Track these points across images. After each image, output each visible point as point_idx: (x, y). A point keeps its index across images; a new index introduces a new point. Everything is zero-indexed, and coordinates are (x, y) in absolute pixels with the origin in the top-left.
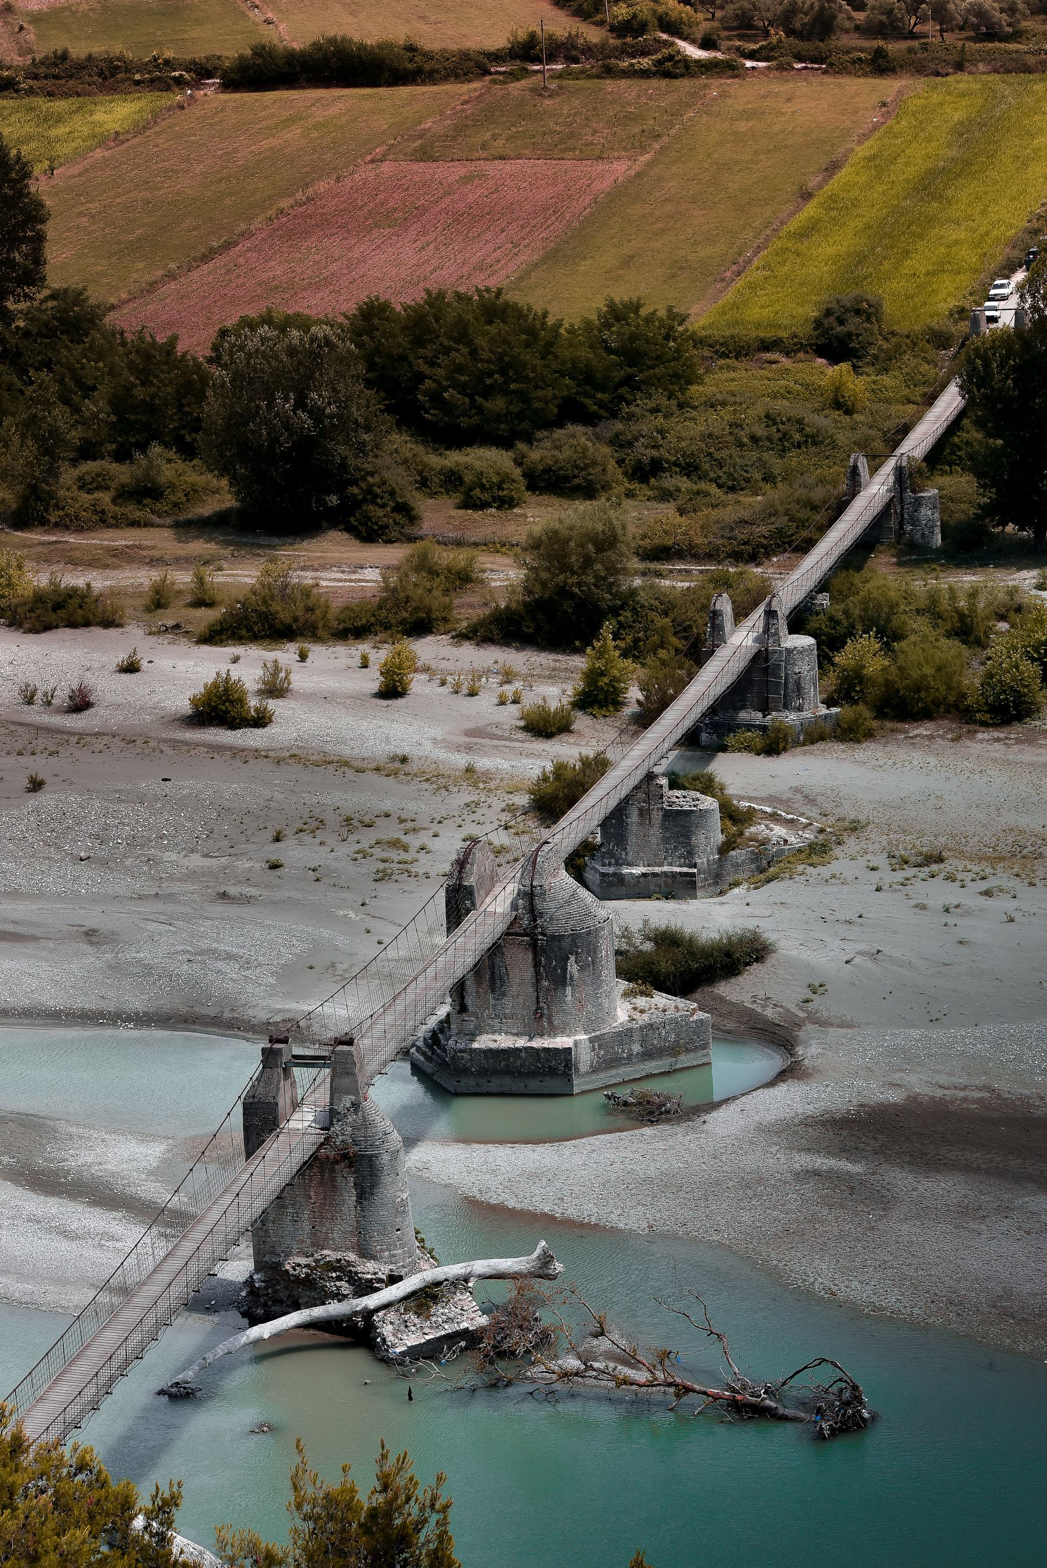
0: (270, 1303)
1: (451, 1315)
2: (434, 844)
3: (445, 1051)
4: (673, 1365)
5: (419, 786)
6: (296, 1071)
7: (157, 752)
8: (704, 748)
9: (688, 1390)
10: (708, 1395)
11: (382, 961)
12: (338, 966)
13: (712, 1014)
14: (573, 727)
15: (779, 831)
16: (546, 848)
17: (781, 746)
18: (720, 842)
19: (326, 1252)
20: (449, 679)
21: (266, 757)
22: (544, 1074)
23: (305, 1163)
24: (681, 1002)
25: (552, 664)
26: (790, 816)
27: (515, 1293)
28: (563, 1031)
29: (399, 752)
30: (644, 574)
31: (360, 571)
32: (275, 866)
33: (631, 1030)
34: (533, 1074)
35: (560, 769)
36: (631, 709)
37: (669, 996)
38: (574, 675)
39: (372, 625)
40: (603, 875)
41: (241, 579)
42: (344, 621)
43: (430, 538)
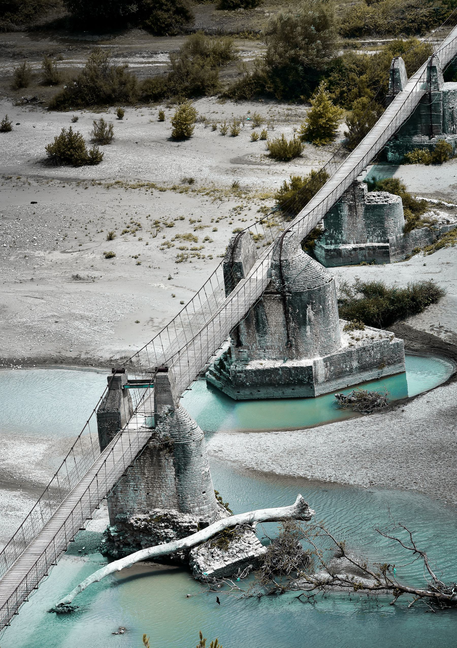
0: (121, 546)
1: (242, 548)
2: (213, 236)
3: (228, 372)
4: (391, 574)
5: (202, 198)
6: (131, 391)
7: (27, 185)
8: (391, 163)
9: (403, 591)
10: (417, 594)
11: (184, 315)
12: (155, 320)
13: (404, 339)
14: (303, 153)
15: (444, 215)
16: (288, 235)
17: (442, 158)
18: (404, 224)
19: (157, 510)
20: (218, 126)
21: (100, 184)
22: (295, 384)
23: (140, 451)
24: (383, 332)
25: (286, 112)
26: (450, 205)
27: (283, 531)
28: (306, 355)
29: (188, 176)
30: (345, 47)
31: (154, 56)
32: (110, 256)
33: (351, 352)
34: (288, 385)
35: (296, 182)
36: (339, 140)
37: (375, 329)
38: (301, 119)
39: (165, 92)
40: (327, 251)
41: (76, 65)
42: (146, 91)
43: (200, 31)
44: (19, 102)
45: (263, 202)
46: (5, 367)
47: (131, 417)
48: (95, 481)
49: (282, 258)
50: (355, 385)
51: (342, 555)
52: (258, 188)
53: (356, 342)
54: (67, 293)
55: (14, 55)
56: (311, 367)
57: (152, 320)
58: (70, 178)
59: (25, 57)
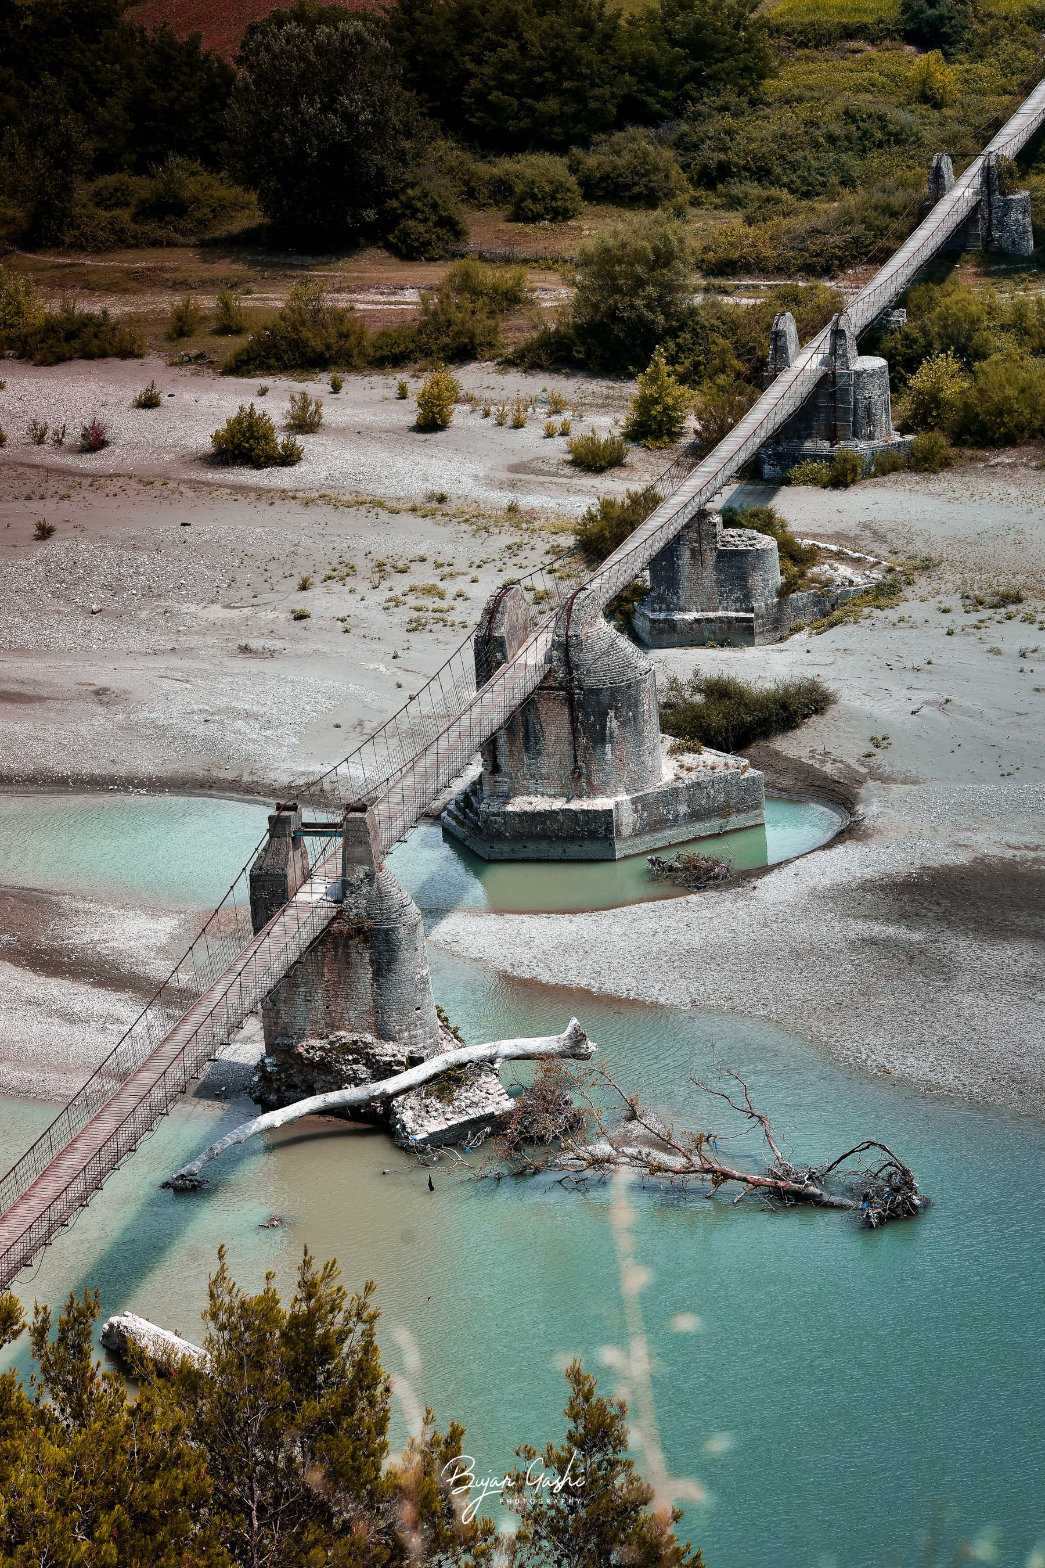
0: (283, 1088)
1: (475, 1099)
2: (472, 591)
3: (477, 814)
5: (457, 528)
6: (307, 840)
7: (176, 495)
8: (768, 481)
9: (727, 1176)
12: (367, 724)
14: (627, 460)
15: (845, 571)
16: (582, 595)
17: (849, 478)
18: (779, 584)
19: (341, 1033)
20: (493, 409)
21: (294, 498)
22: (583, 838)
23: (316, 939)
24: (731, 759)
25: (605, 392)
26: (857, 555)
28: (604, 790)
29: (437, 490)
31: (400, 292)
32: (300, 617)
33: (676, 790)
34: (572, 838)
36: (686, 441)
37: (719, 753)
39: (411, 352)
40: (654, 621)
41: (271, 303)
42: (381, 348)
44: (176, 359)
45: (555, 537)
46: (120, 791)
47: (305, 882)
48: (237, 983)
49: (570, 633)
50: (683, 843)
51: (632, 1117)
52: (549, 515)
53: (686, 772)
54: (227, 675)
55: (175, 284)
56: (611, 810)
57: (361, 723)
58: (247, 487)
59: (192, 288)
